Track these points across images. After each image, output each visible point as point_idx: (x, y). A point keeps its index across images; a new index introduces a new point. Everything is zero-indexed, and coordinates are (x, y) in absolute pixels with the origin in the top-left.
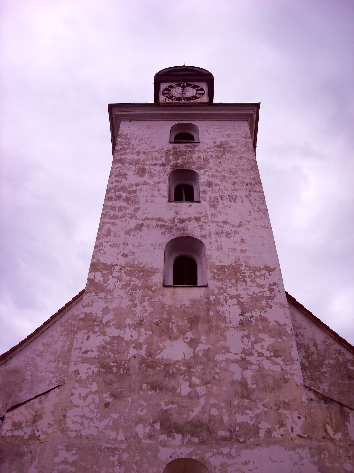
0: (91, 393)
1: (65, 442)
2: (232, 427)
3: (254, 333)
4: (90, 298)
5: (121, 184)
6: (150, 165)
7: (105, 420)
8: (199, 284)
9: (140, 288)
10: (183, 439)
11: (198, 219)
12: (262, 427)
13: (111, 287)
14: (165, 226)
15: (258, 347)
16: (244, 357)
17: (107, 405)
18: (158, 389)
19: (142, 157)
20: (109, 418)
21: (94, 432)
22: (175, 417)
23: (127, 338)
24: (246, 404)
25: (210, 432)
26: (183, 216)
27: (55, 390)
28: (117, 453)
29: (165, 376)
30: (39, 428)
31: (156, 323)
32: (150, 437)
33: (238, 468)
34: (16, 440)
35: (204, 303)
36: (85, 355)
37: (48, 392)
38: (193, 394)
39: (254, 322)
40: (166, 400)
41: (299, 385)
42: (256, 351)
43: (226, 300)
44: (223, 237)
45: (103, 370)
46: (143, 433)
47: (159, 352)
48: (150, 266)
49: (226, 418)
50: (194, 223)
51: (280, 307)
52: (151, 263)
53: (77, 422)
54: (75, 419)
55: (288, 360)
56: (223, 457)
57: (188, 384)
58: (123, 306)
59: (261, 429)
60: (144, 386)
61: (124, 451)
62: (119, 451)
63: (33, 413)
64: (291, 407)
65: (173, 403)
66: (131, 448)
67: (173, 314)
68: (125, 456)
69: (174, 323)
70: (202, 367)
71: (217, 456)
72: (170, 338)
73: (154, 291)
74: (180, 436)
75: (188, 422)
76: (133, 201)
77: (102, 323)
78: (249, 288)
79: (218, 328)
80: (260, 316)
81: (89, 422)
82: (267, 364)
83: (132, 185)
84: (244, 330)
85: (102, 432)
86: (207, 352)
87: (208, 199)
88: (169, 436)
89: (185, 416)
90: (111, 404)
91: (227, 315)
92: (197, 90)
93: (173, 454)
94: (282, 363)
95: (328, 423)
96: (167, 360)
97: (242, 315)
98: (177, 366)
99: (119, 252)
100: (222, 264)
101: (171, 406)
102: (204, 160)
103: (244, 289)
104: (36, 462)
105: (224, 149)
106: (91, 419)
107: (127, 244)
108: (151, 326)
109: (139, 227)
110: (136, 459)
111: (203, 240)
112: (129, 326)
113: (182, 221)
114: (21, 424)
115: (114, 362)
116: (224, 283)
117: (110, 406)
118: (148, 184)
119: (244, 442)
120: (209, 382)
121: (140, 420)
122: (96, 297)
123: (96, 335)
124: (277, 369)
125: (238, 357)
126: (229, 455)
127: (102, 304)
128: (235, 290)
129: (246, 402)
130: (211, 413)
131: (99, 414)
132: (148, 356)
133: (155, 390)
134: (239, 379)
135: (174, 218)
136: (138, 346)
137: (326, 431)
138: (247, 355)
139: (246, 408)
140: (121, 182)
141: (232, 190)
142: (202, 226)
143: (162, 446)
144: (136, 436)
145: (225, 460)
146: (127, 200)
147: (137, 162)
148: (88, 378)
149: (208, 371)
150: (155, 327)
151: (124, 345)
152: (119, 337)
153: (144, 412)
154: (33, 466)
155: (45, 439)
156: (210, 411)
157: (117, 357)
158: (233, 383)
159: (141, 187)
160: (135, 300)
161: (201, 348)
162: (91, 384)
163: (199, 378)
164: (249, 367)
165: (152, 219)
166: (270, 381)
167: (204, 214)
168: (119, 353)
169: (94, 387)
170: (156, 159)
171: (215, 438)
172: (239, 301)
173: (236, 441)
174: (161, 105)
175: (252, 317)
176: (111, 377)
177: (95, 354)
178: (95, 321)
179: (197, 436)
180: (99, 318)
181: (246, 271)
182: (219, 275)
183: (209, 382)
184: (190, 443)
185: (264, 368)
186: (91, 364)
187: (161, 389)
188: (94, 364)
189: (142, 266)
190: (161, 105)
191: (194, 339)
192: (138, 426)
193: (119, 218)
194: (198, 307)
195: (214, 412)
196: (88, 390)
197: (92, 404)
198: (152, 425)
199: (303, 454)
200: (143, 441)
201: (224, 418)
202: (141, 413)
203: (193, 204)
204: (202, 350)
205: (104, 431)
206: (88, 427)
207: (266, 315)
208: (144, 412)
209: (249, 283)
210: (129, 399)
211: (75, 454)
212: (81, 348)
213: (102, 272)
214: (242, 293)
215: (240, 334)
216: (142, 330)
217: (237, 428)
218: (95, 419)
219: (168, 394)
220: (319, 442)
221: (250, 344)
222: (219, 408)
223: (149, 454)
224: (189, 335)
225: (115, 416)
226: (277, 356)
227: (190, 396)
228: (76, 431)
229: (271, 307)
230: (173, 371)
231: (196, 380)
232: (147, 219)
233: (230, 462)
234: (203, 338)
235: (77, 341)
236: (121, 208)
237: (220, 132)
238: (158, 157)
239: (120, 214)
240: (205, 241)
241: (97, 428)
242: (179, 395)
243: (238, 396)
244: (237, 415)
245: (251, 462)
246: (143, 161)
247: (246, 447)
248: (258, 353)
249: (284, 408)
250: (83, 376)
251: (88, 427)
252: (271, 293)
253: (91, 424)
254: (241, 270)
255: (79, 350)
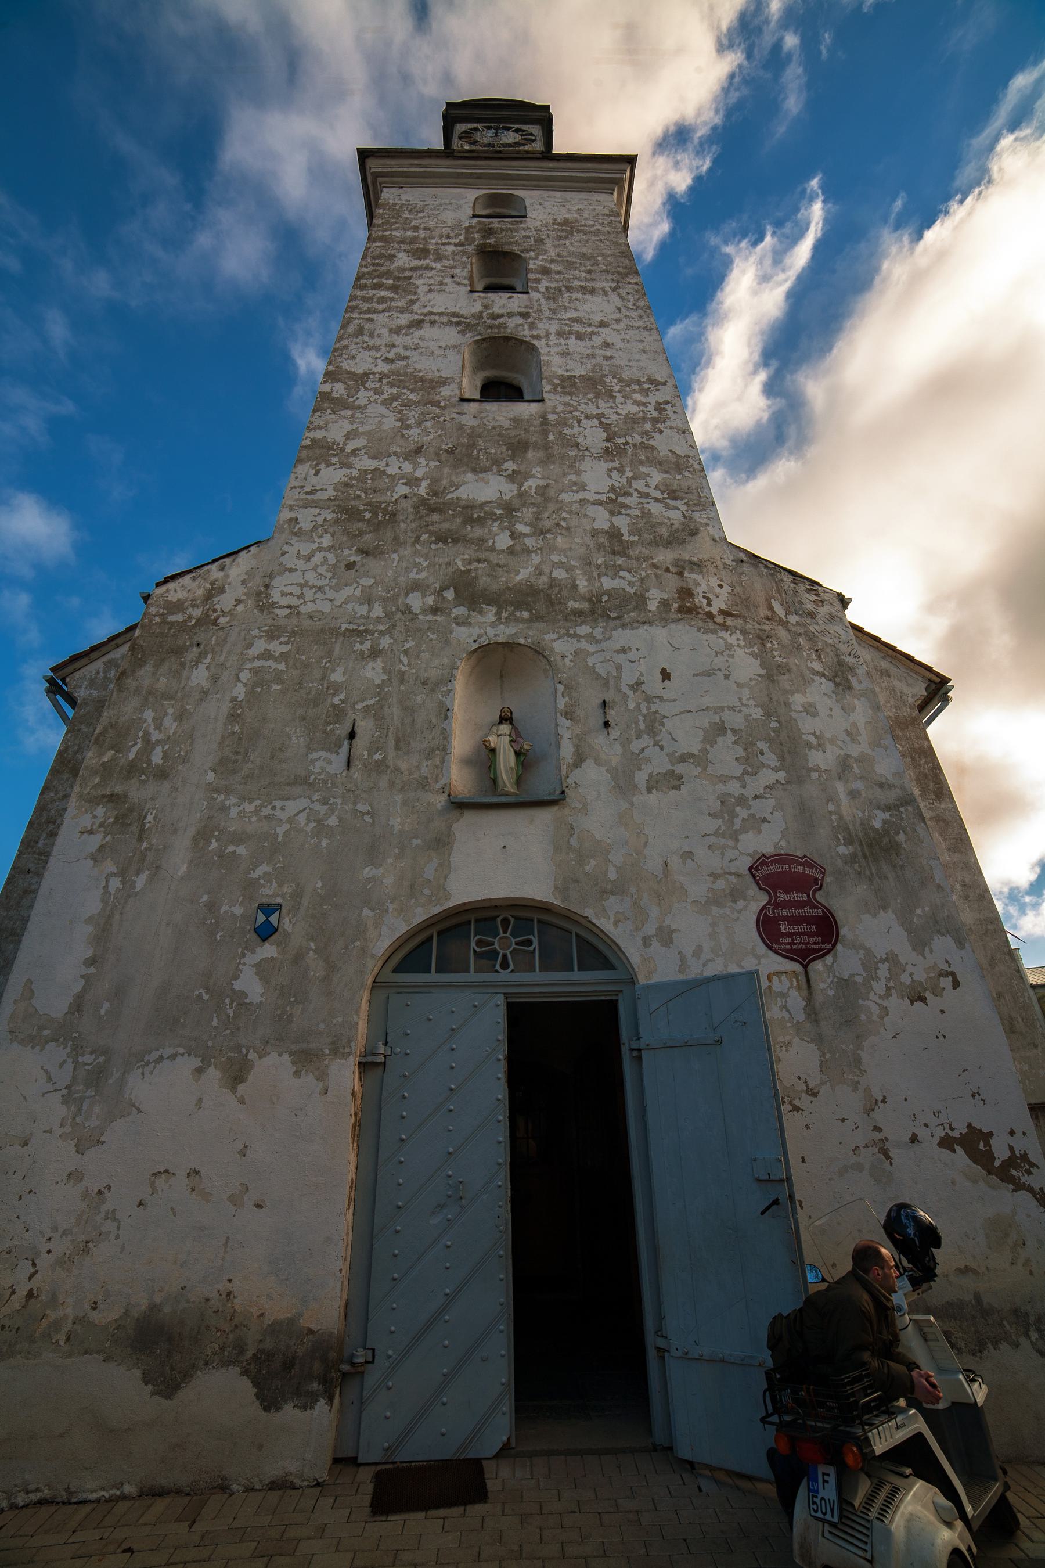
0: (320, 549)
1: (266, 625)
2: (593, 596)
3: (631, 466)
4: (322, 418)
5: (384, 268)
6: (437, 244)
7: (347, 588)
8: (526, 397)
9: (417, 404)
10: (498, 614)
11: (525, 315)
12: (651, 597)
13: (362, 402)
14: (465, 323)
15: (639, 485)
16: (614, 497)
17: (350, 566)
18: (449, 540)
19: (422, 234)
20: (355, 585)
21: (327, 607)
22: (484, 581)
23: (390, 471)
24: (619, 562)
25: (550, 602)
26: (496, 310)
27: (251, 549)
28: (369, 637)
29: (464, 523)
30: (218, 607)
31: (446, 451)
32: (435, 610)
33: (609, 658)
34: (170, 629)
35: (537, 423)
36: (309, 497)
37: (237, 552)
38: (518, 548)
39: (630, 451)
40: (467, 556)
41: (718, 539)
42: (636, 490)
43: (579, 422)
44: (572, 340)
45: (344, 516)
46: (421, 605)
47: (452, 490)
48: (437, 374)
49: (582, 584)
50: (519, 320)
51: (678, 432)
52: (438, 370)
53: (291, 594)
54: (288, 589)
55: (695, 505)
56: (579, 641)
57: (508, 533)
58: (385, 427)
59: (650, 599)
60: (425, 537)
61: (382, 633)
62: (373, 635)
63: (209, 586)
64: (705, 570)
65: (479, 561)
66: (397, 629)
67: (480, 437)
68: (385, 642)
69: (481, 449)
70: (535, 509)
71: (566, 638)
72: (474, 471)
73: (444, 408)
74: (494, 610)
75: (508, 588)
76: (404, 291)
77: (344, 451)
78: (619, 405)
79: (563, 457)
80: (642, 443)
81: (315, 593)
82: (655, 508)
83: (404, 270)
84: (613, 461)
85: (340, 606)
86: (542, 491)
87: (543, 290)
88: (471, 609)
89: (503, 579)
90: (359, 564)
91: (580, 440)
92: (522, 135)
93: (480, 636)
94: (684, 508)
95: (774, 597)
96: (468, 500)
97: (608, 440)
98: (487, 508)
99: (378, 356)
100: (569, 374)
101: (475, 565)
102: (536, 241)
103: (612, 407)
104: (208, 660)
105: (572, 228)
106: (320, 588)
107: (394, 346)
108: (437, 454)
109: (419, 323)
110: (407, 646)
111: (535, 342)
112: (395, 454)
113: (494, 317)
114: (183, 603)
115: (366, 505)
116: (574, 398)
117: (356, 567)
118: (432, 269)
119: (618, 618)
120: (549, 530)
121: (416, 586)
122: (333, 416)
123: (332, 468)
124: (676, 516)
125: (603, 498)
126: (591, 638)
127: (347, 426)
128: (594, 408)
129: (620, 561)
130: (554, 575)
131: (335, 581)
132: (432, 496)
133: (445, 542)
134: (606, 528)
135: (481, 312)
136: (413, 482)
137: (771, 608)
138: (618, 495)
139: (621, 568)
140: (382, 265)
141: (586, 279)
142: (533, 323)
143: (458, 624)
144: (408, 610)
145: (584, 645)
146: (394, 289)
147: (413, 241)
148: (315, 528)
149: (546, 515)
150: (444, 456)
151: (387, 481)
152: (376, 470)
153: (424, 575)
154: (202, 667)
155: (227, 623)
156: (551, 573)
157: (372, 498)
158: (595, 533)
159: (420, 273)
160: (408, 419)
161: (531, 484)
162: (321, 537)
163: (530, 525)
164: (623, 512)
165: (441, 314)
166: (664, 532)
167: (535, 308)
168: (375, 491)
169: (326, 541)
170: (448, 237)
171: (562, 612)
172: (601, 423)
173: (602, 616)
174: (455, 154)
175: (627, 443)
176: (361, 525)
177: (331, 493)
178: (330, 448)
179: (526, 610)
180: (338, 444)
181: (613, 384)
182: (563, 387)
183: (549, 531)
184: (512, 619)
185: (651, 514)
186: (321, 508)
187: (456, 541)
188: (329, 508)
189: (421, 374)
190: (455, 154)
191: (520, 471)
192: (411, 595)
193: (378, 312)
194: (525, 429)
195: (560, 574)
196: (315, 546)
197: (322, 565)
198: (439, 593)
199: (732, 640)
200: (420, 617)
201: (578, 582)
202: (417, 577)
203: (515, 295)
204: (534, 486)
205: (344, 606)
206: (314, 601)
207: (652, 442)
208: (424, 575)
209: (619, 399)
210: (395, 556)
211: (286, 643)
212: (302, 487)
213: (345, 383)
214: (609, 412)
215: (604, 466)
216: (422, 461)
217: (605, 598)
218: (327, 589)
219: (469, 548)
220: (759, 624)
221: (624, 481)
222: (569, 569)
223: (434, 637)
224: (510, 466)
225: (367, 582)
226: (675, 498)
227: (511, 551)
228: (289, 607)
229: (661, 432)
230: (479, 516)
231: (521, 528)
232: (431, 313)
233: (591, 648)
234: (537, 471)
235: (296, 478)
236: (382, 300)
237: (564, 206)
238: (452, 235)
239: (381, 307)
240: (540, 344)
241: (331, 600)
242: (492, 549)
243: (605, 551)
244: (604, 579)
245: (634, 650)
246: (425, 239)
247: (623, 626)
248: (639, 492)
249: (692, 571)
250: (306, 524)
251: (314, 601)
252: (660, 413)
253: (319, 595)
254: (605, 382)
255: (299, 490)
